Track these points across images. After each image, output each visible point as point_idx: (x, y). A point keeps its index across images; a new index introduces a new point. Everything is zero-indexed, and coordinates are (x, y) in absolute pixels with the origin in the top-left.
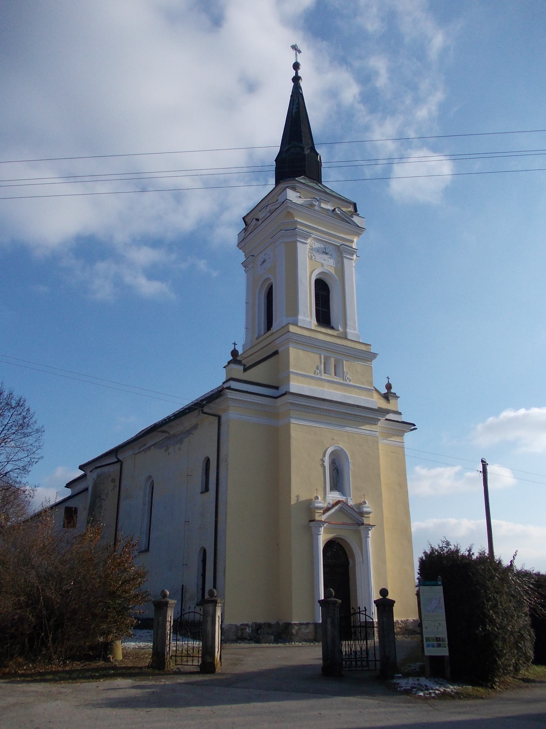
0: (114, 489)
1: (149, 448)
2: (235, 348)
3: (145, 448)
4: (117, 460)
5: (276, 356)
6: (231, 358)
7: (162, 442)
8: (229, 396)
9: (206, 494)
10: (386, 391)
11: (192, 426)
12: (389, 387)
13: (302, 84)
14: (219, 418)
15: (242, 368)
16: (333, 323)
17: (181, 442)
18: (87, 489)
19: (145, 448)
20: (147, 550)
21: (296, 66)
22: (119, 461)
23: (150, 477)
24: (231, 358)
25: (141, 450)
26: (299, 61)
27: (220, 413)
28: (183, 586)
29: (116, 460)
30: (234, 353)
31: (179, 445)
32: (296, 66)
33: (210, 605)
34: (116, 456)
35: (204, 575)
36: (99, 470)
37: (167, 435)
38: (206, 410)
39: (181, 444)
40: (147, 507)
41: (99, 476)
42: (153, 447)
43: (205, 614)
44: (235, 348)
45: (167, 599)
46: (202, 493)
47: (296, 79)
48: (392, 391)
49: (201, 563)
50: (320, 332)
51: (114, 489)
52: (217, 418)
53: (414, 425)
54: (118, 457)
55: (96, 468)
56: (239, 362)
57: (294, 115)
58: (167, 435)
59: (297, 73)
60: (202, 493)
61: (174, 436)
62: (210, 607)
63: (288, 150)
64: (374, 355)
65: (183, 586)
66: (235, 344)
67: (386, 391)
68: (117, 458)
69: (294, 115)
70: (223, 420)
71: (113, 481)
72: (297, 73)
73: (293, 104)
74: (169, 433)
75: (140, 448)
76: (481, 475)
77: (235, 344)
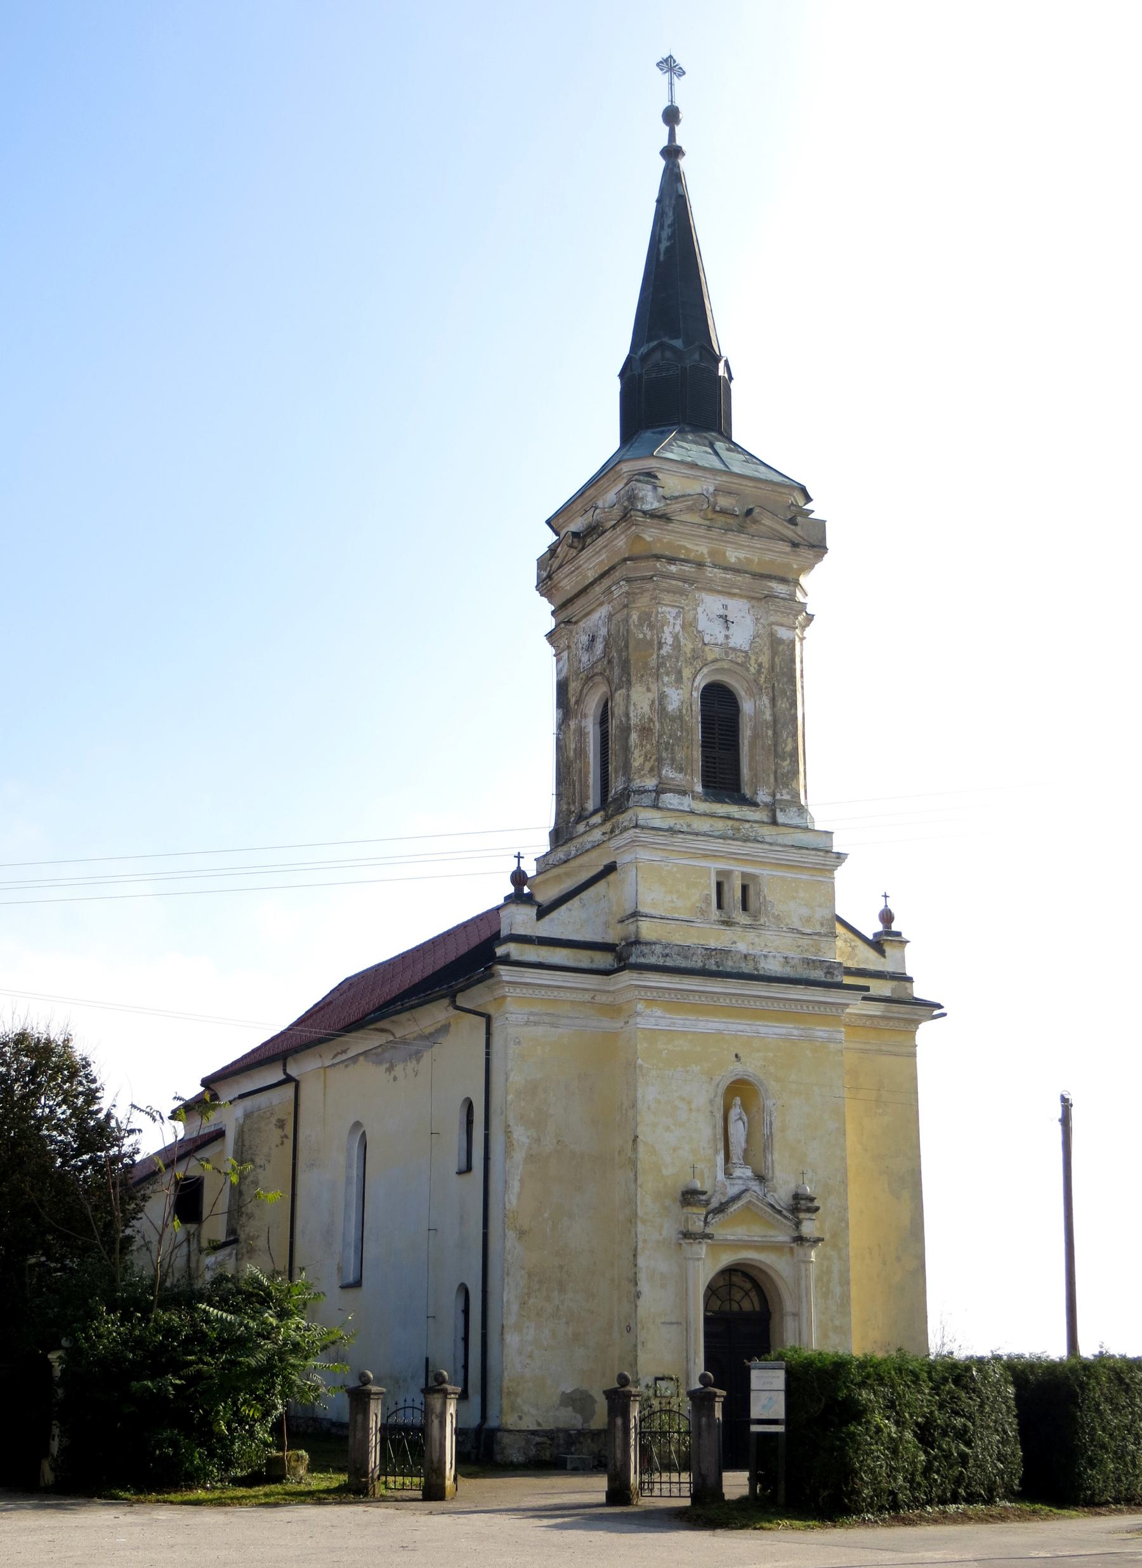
0: (282, 1143)
1: (354, 1059)
2: (519, 867)
3: (344, 1057)
4: (284, 1077)
5: (612, 877)
6: (511, 889)
7: (379, 1050)
8: (504, 978)
9: (467, 1178)
10: (879, 927)
11: (438, 1025)
12: (887, 917)
13: (684, 163)
14: (489, 1019)
15: (532, 911)
16: (747, 791)
17: (417, 1055)
18: (219, 1134)
19: (344, 1057)
20: (358, 1284)
21: (671, 116)
22: (289, 1079)
23: (357, 1125)
24: (511, 889)
25: (336, 1061)
26: (676, 104)
27: (491, 1011)
28: (427, 1359)
29: (282, 1077)
30: (519, 878)
31: (415, 1062)
32: (671, 116)
33: (436, 1396)
34: (285, 1070)
35: (466, 1339)
36: (248, 1103)
37: (391, 1038)
38: (461, 1001)
39: (418, 1061)
40: (354, 1190)
41: (247, 1116)
42: (361, 1058)
43: (427, 1411)
44: (519, 867)
45: (446, 1386)
46: (460, 1173)
47: (672, 180)
48: (895, 927)
49: (461, 1316)
50: (712, 815)
51: (282, 1143)
52: (484, 1020)
53: (939, 1006)
54: (288, 1071)
55: (242, 1096)
56: (528, 899)
57: (662, 258)
58: (391, 1038)
59: (672, 136)
60: (460, 1173)
61: (404, 1041)
62: (436, 1401)
63: (645, 358)
64: (840, 857)
65: (427, 1359)
66: (519, 857)
67: (879, 927)
68: (285, 1073)
69: (662, 258)
70: (496, 1025)
71: (281, 1124)
72: (672, 136)
73: (662, 227)
74: (393, 1034)
75: (335, 1056)
76: (1058, 1127)
77: (519, 857)
